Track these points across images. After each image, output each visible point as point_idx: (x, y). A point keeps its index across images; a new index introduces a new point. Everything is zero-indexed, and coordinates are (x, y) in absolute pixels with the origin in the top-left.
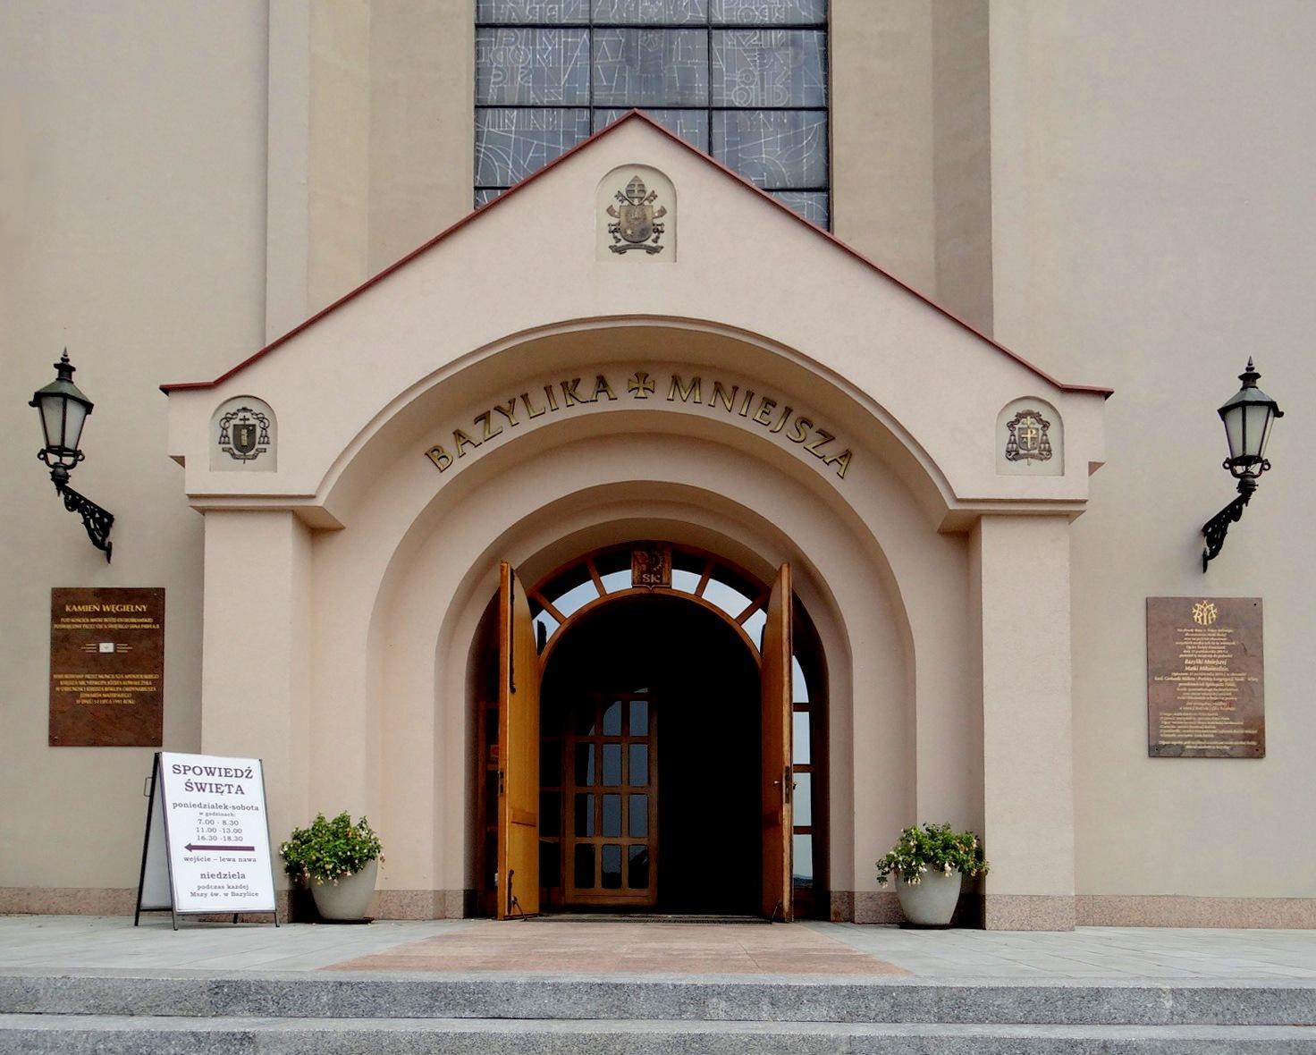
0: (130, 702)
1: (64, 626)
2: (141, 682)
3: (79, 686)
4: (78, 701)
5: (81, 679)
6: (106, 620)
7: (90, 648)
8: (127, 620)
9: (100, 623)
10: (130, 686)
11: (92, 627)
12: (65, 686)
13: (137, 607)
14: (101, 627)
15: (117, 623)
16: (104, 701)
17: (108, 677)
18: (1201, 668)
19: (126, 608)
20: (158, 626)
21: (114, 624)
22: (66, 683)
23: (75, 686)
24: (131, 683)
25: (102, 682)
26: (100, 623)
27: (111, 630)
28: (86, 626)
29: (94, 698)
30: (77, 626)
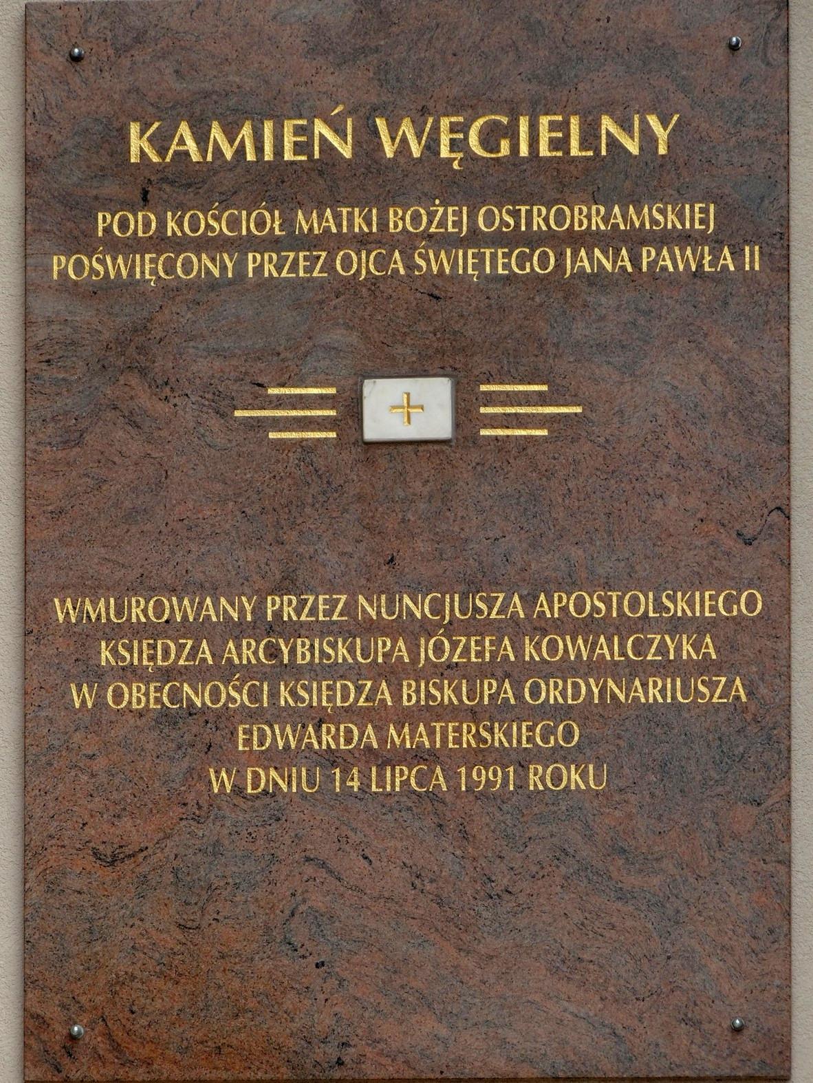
0: (573, 777)
1: (115, 267)
2: (652, 642)
3: (227, 672)
4: (221, 781)
5: (238, 630)
6: (399, 220)
7: (293, 412)
8: (540, 218)
9: (362, 242)
10: (566, 669)
11: (301, 266)
12: (131, 673)
13: (607, 124)
14: (365, 264)
15: (474, 238)
16: (400, 777)
17: (421, 609)
18: (427, 650)
19: (536, 136)
20: (63, 610)
21: (455, 245)
22: (138, 654)
23: (198, 675)
24: (574, 648)
25: (382, 645)
26: (362, 242)
27: (436, 291)
28: (265, 264)
29: (331, 758)
30: (205, 264)
